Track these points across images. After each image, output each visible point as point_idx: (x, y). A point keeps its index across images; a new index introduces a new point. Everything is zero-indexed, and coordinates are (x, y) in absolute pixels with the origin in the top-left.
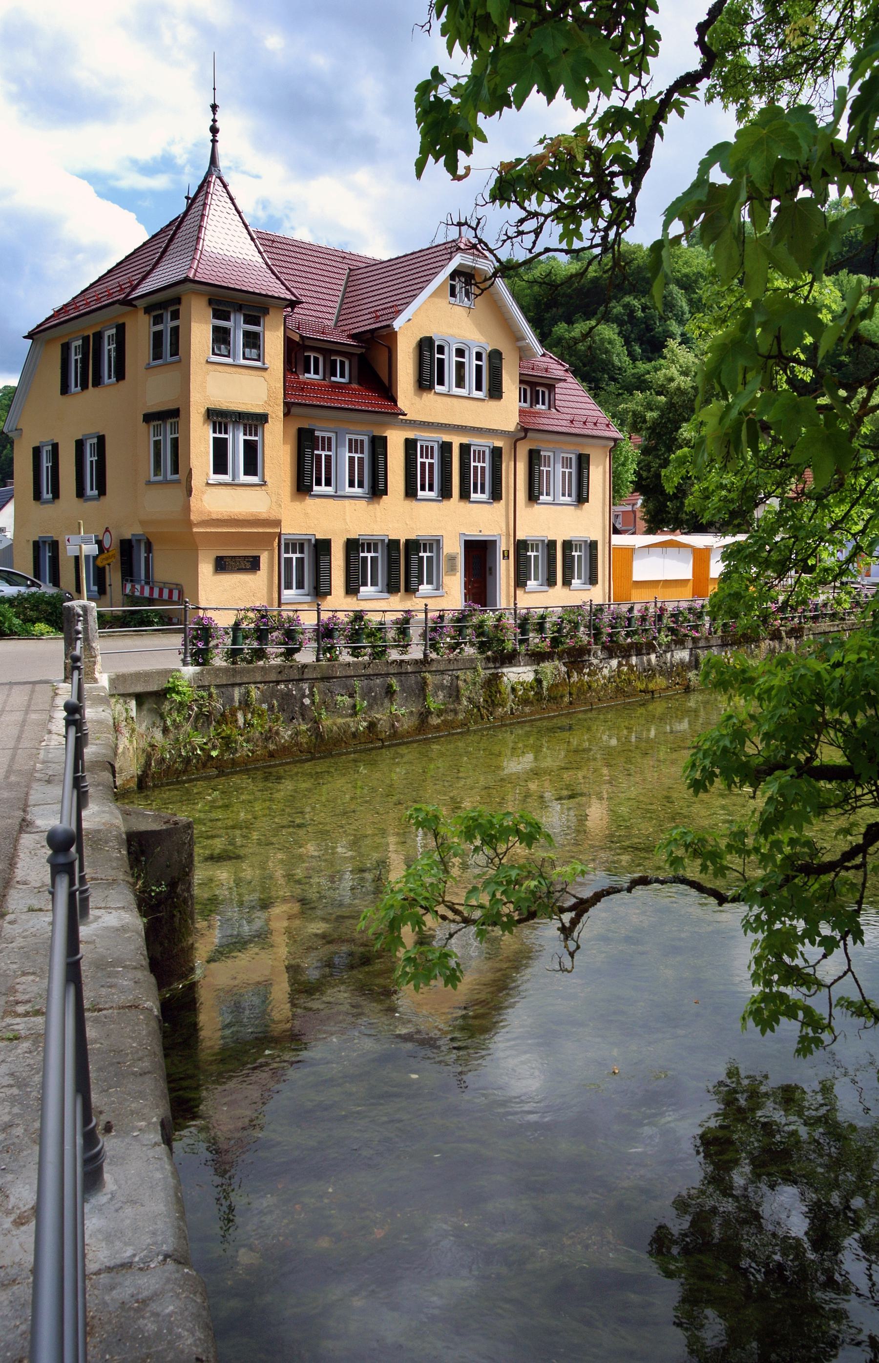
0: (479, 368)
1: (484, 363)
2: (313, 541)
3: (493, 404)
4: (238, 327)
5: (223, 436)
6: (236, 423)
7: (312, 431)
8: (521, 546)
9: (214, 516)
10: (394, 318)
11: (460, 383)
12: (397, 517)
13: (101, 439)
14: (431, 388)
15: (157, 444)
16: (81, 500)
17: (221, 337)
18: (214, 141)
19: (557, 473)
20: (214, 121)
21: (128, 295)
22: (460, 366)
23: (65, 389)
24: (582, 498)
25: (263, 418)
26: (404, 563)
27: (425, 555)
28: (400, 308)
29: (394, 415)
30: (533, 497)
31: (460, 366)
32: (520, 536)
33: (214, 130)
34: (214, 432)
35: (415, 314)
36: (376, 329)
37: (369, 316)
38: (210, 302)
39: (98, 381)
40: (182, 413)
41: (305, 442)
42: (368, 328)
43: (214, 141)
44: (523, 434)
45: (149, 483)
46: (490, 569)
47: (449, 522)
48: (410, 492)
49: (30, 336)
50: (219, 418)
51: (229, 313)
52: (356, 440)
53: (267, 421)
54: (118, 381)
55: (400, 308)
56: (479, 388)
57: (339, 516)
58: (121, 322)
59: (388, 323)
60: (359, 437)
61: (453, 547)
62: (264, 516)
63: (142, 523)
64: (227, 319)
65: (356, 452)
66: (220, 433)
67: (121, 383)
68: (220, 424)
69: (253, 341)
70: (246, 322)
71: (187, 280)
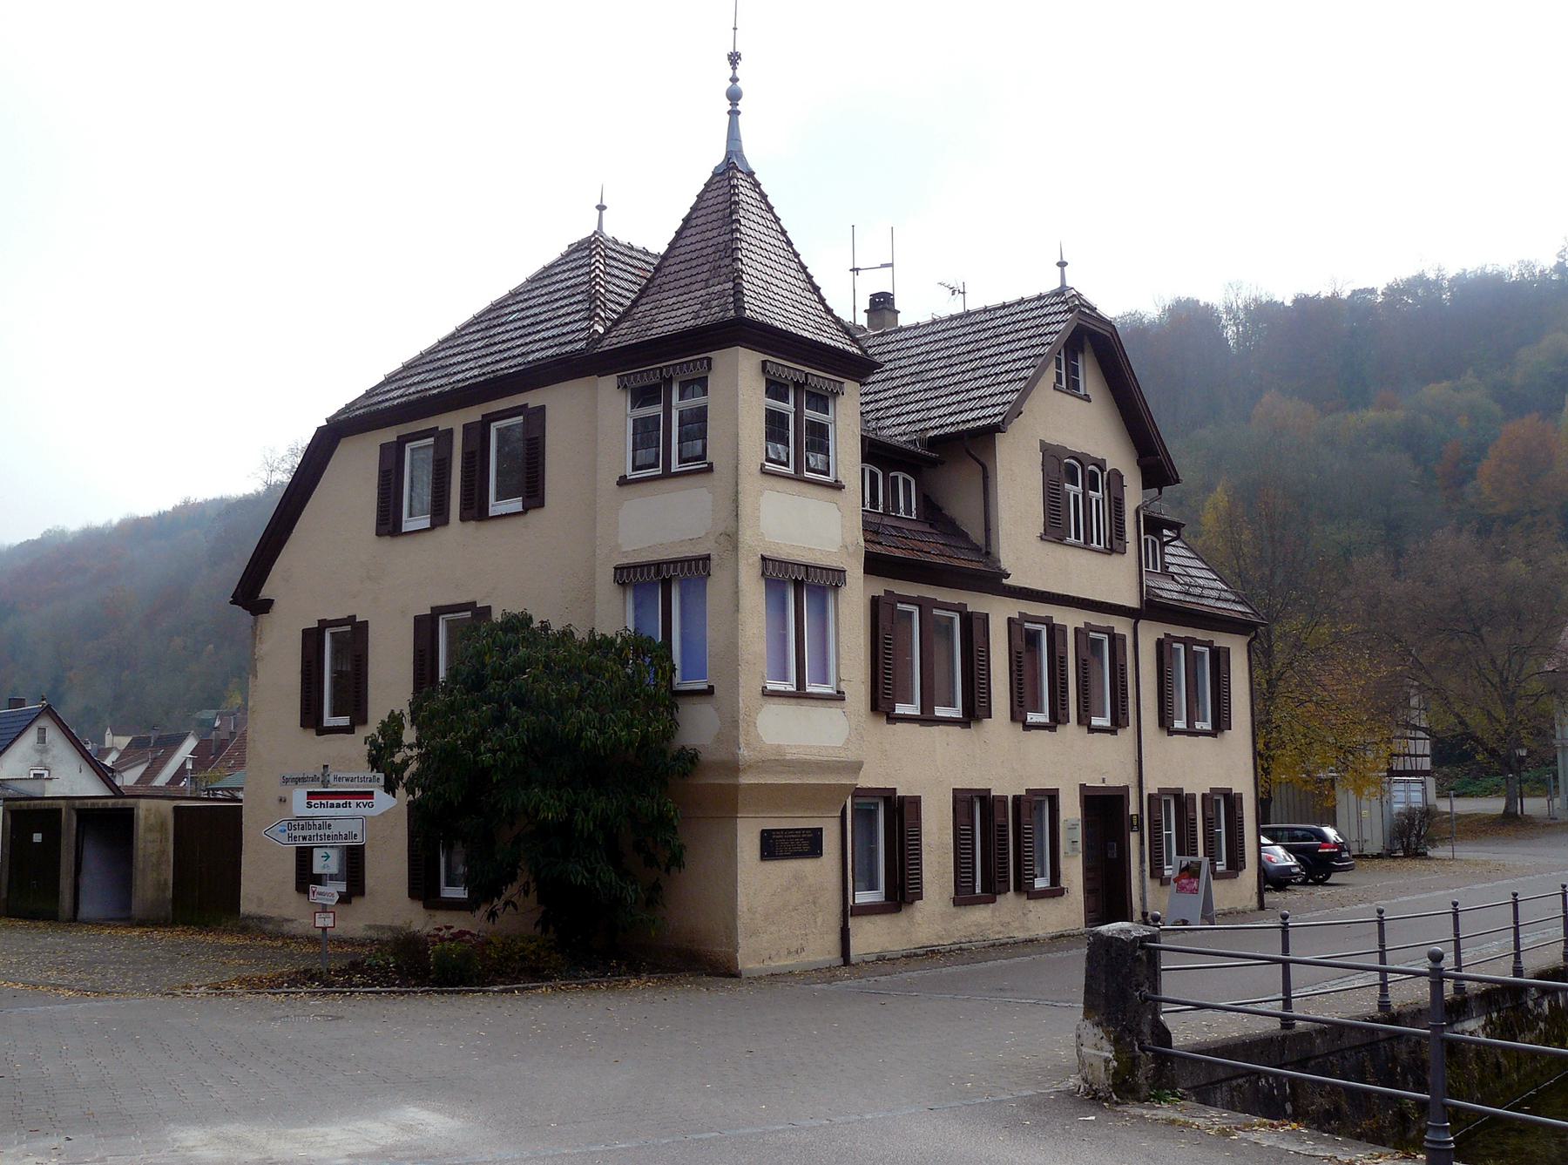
18: (734, 114)
20: (734, 80)
23: (389, 523)
24: (1221, 723)
25: (836, 577)
33: (734, 96)
39: (475, 509)
43: (734, 114)
61: (1071, 810)
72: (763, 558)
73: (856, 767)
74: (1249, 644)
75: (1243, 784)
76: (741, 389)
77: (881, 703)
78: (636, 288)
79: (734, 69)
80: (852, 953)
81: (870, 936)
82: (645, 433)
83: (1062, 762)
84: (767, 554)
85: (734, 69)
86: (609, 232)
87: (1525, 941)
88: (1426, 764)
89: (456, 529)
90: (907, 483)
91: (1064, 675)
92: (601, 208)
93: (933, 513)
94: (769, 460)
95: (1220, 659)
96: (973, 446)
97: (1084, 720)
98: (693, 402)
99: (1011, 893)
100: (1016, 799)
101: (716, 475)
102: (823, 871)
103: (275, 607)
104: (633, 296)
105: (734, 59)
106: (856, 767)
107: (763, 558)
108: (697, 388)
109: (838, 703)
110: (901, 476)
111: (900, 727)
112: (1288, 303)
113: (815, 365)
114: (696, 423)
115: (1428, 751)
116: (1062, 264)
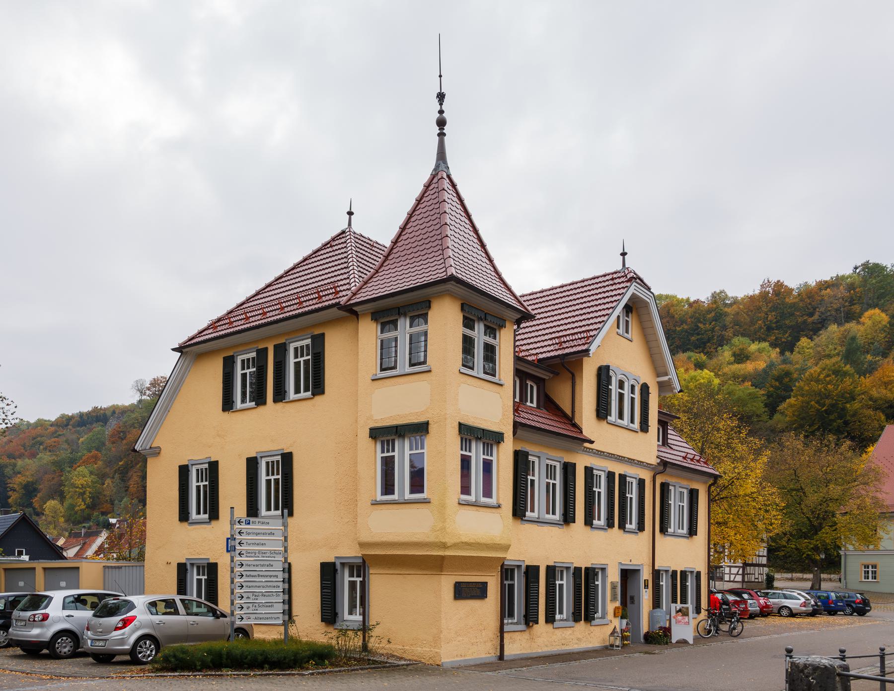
0: (633, 399)
1: (637, 396)
2: (523, 569)
4: (479, 335)
6: (478, 439)
9: (464, 539)
10: (590, 343)
11: (621, 416)
16: (588, 528)
18: (441, 135)
19: (678, 503)
20: (441, 112)
22: (621, 396)
23: (228, 404)
25: (498, 438)
28: (592, 333)
31: (621, 396)
33: (441, 123)
36: (567, 354)
37: (550, 342)
38: (463, 308)
43: (441, 135)
44: (662, 468)
45: (375, 503)
46: (632, 598)
47: (609, 549)
49: (180, 349)
50: (469, 433)
51: (474, 321)
54: (314, 394)
55: (592, 333)
57: (544, 544)
58: (317, 332)
61: (614, 576)
63: (362, 545)
68: (388, 441)
71: (452, 278)
72: (460, 424)
73: (506, 548)
74: (709, 487)
75: (701, 566)
76: (445, 323)
77: (519, 511)
78: (372, 270)
79: (441, 104)
80: (505, 653)
81: (518, 644)
83: (609, 549)
84: (462, 422)
85: (441, 104)
86: (357, 228)
88: (764, 561)
90: (532, 387)
91: (615, 503)
92: (350, 213)
93: (548, 404)
95: (693, 495)
96: (567, 366)
99: (582, 622)
100: (587, 569)
102: (488, 608)
103: (162, 452)
104: (376, 268)
105: (441, 97)
106: (506, 548)
107: (460, 424)
108: (421, 320)
110: (529, 383)
111: (528, 526)
113: (488, 310)
114: (417, 343)
115: (765, 554)
116: (624, 254)
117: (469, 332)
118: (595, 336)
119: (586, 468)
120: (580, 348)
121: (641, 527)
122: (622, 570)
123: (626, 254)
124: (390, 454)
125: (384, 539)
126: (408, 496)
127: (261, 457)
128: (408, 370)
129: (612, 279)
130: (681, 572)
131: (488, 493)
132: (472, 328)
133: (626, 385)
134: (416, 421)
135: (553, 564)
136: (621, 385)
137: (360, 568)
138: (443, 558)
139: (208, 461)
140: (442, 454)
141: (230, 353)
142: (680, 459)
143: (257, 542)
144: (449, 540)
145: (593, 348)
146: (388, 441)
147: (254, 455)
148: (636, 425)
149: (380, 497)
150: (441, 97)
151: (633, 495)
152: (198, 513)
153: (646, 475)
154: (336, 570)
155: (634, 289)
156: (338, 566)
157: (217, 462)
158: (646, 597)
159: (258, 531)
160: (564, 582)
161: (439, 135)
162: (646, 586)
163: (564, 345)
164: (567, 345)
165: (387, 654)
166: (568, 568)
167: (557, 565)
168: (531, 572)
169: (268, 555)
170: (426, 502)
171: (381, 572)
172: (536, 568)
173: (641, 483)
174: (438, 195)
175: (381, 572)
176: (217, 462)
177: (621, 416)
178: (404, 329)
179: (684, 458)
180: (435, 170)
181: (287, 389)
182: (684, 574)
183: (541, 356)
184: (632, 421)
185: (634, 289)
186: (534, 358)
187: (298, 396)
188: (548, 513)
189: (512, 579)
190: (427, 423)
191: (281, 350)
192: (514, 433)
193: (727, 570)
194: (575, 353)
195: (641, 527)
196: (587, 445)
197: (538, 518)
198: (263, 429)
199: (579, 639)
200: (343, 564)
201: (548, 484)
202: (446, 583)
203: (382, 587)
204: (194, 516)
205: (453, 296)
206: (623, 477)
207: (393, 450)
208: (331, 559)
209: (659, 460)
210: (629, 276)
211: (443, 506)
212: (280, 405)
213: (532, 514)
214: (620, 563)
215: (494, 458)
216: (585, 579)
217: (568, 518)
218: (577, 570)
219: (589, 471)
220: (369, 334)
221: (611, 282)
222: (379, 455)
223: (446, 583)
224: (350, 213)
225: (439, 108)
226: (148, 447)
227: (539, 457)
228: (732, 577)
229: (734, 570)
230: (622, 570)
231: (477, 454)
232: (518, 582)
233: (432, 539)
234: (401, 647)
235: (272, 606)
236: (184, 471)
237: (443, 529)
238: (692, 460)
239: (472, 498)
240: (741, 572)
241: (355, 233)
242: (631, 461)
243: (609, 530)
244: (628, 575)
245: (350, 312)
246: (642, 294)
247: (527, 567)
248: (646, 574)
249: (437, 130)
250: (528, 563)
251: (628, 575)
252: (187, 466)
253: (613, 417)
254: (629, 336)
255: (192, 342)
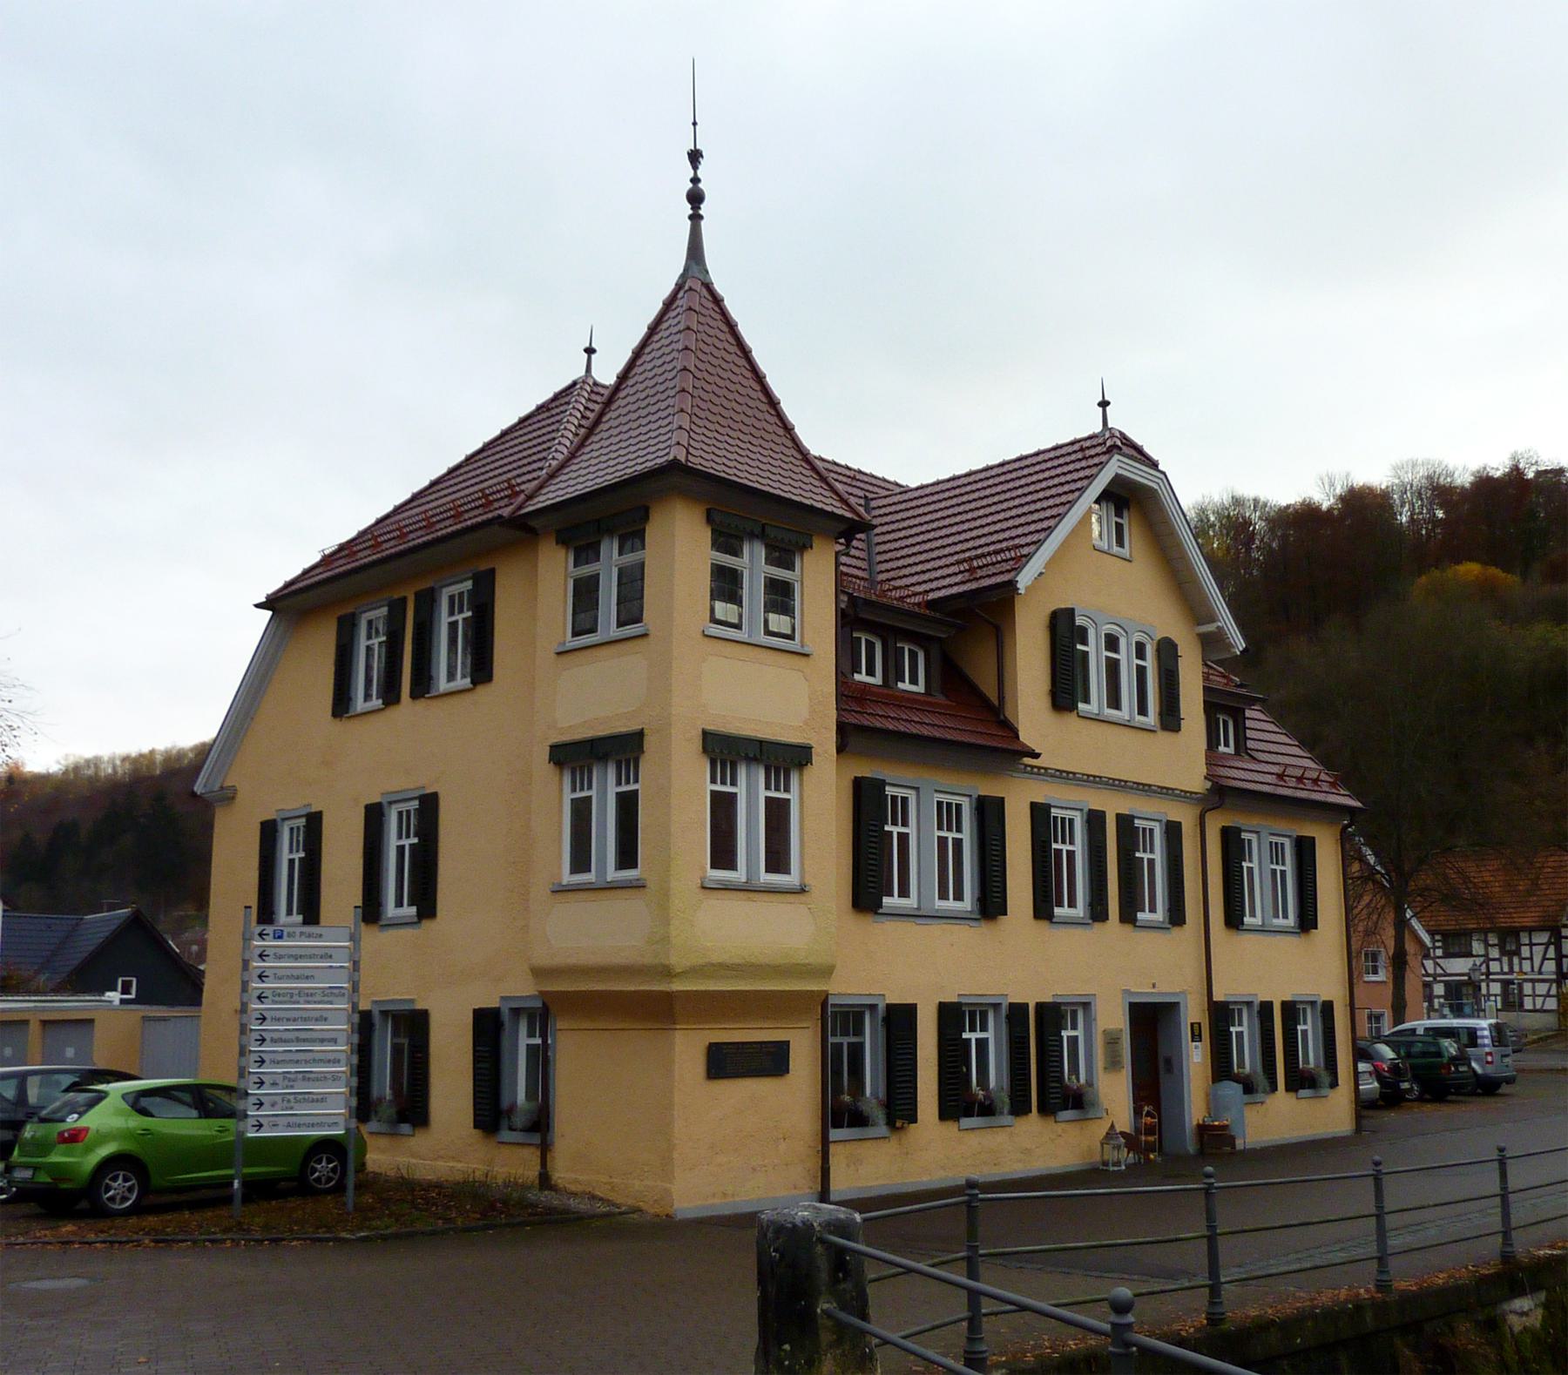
0: (1141, 671)
1: (1150, 663)
2: (882, 1007)
3: (1165, 737)
4: (753, 564)
5: (728, 789)
6: (751, 760)
7: (882, 784)
8: (1221, 1014)
9: (716, 958)
10: (1018, 570)
11: (1115, 702)
12: (1022, 960)
13: (429, 806)
14: (1071, 707)
15: (581, 811)
17: (726, 584)
18: (696, 218)
19: (1263, 868)
21: (520, 508)
22: (1113, 668)
23: (341, 704)
24: (1307, 921)
25: (800, 756)
26: (1034, 1056)
27: (972, 1036)
28: (1025, 551)
29: (1008, 752)
30: (1234, 920)
31: (1113, 668)
32: (1218, 996)
33: (695, 198)
34: (713, 781)
35: (1048, 565)
39: (423, 685)
40: (650, 742)
41: (869, 810)
42: (955, 590)
43: (696, 218)
45: (561, 890)
46: (1168, 1061)
47: (1096, 967)
48: (1043, 909)
49: (270, 603)
50: (725, 751)
52: (949, 805)
53: (809, 761)
54: (475, 683)
55: (1025, 551)
56: (1143, 710)
57: (928, 959)
58: (484, 566)
59: (1006, 577)
60: (955, 799)
61: (1113, 1018)
62: (801, 958)
63: (539, 973)
64: (736, 552)
65: (950, 829)
66: (723, 783)
67: (482, 690)
69: (780, 597)
70: (769, 561)
71: (674, 465)
76: (681, 547)
79: (695, 168)
82: (585, 594)
83: (1096, 967)
84: (709, 727)
85: (695, 168)
87: (1394, 1242)
89: (407, 707)
91: (1115, 873)
92: (590, 351)
94: (714, 621)
95: (1305, 851)
97: (1128, 917)
98: (630, 558)
101: (651, 639)
102: (795, 1095)
103: (239, 796)
105: (695, 157)
106: (826, 972)
107: (705, 734)
109: (802, 898)
111: (890, 926)
112: (1467, 485)
116: (1104, 404)
117: (727, 560)
118: (1029, 556)
119: (1034, 806)
120: (999, 579)
121: (1176, 916)
122: (1132, 1005)
123: (1100, 404)
124: (632, 787)
125: (572, 961)
126: (612, 874)
127: (390, 803)
128: (615, 632)
129: (1082, 449)
130: (1284, 1004)
131: (777, 860)
132: (736, 552)
133: (1123, 642)
134: (624, 730)
135: (955, 1000)
136: (1112, 643)
137: (541, 1015)
138: (669, 997)
139: (304, 812)
140: (680, 792)
141: (350, 610)
142: (1269, 779)
143: (295, 973)
144: (677, 961)
145: (1024, 580)
146: (582, 768)
147: (378, 800)
148: (1152, 719)
149: (567, 878)
150: (695, 157)
151: (1157, 855)
152: (399, 904)
153: (1185, 816)
154: (502, 1024)
155: (1115, 467)
156: (506, 1016)
157: (320, 813)
158: (1196, 1057)
159: (299, 952)
160: (989, 1035)
161: (691, 217)
162: (1197, 1036)
163: (979, 573)
164: (984, 572)
165: (584, 1193)
166: (996, 1006)
167: (964, 1000)
168: (900, 1019)
169: (317, 998)
170: (638, 886)
171: (585, 1026)
172: (1023, 1007)
173: (1173, 831)
174: (695, 321)
175: (585, 1026)
176: (320, 813)
177: (1115, 702)
178: (610, 561)
179: (1280, 776)
180: (682, 276)
181: (434, 673)
182: (1291, 1011)
183: (931, 596)
184: (1143, 710)
185: (1115, 467)
186: (917, 599)
187: (453, 686)
188: (943, 895)
189: (859, 1031)
190: (639, 735)
191: (427, 602)
192: (841, 749)
193: (1527, 988)
194: (997, 586)
195: (1176, 916)
196: (1027, 760)
197: (918, 909)
198: (398, 748)
199: (1027, 1151)
200: (516, 1012)
201: (942, 842)
202: (688, 1049)
203: (579, 1057)
204: (391, 910)
205: (690, 496)
206: (1125, 822)
207: (590, 787)
208: (491, 1002)
209: (1209, 785)
210: (1109, 443)
211: (665, 894)
212: (421, 704)
213: (903, 902)
214: (1127, 992)
215: (793, 796)
216: (1040, 1030)
217: (991, 905)
218: (1017, 1012)
219: (1040, 813)
220: (553, 572)
221: (1080, 455)
222: (568, 796)
223: (688, 1049)
224: (590, 351)
225: (691, 174)
226: (217, 788)
227: (917, 789)
228: (1539, 1001)
229: (1542, 988)
230: (1132, 1005)
231: (751, 791)
232: (871, 1040)
233: (648, 960)
234: (604, 1179)
235: (323, 1100)
236: (269, 831)
237: (666, 939)
238: (1300, 779)
239: (738, 876)
240: (1554, 991)
241: (596, 384)
242: (1144, 789)
243: (1097, 925)
244: (1151, 1020)
245: (523, 531)
246: (1137, 473)
247: (890, 1007)
248: (1193, 1012)
249: (687, 209)
250: (894, 999)
251: (1151, 1020)
252: (274, 822)
253: (1097, 702)
254: (1125, 552)
255: (301, 585)
